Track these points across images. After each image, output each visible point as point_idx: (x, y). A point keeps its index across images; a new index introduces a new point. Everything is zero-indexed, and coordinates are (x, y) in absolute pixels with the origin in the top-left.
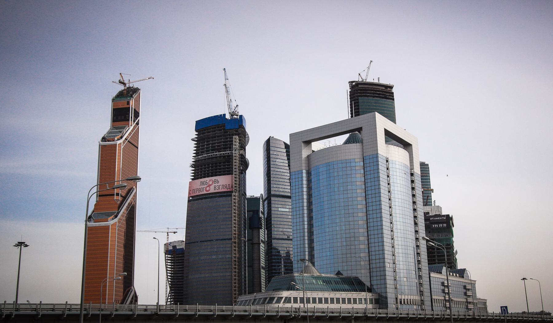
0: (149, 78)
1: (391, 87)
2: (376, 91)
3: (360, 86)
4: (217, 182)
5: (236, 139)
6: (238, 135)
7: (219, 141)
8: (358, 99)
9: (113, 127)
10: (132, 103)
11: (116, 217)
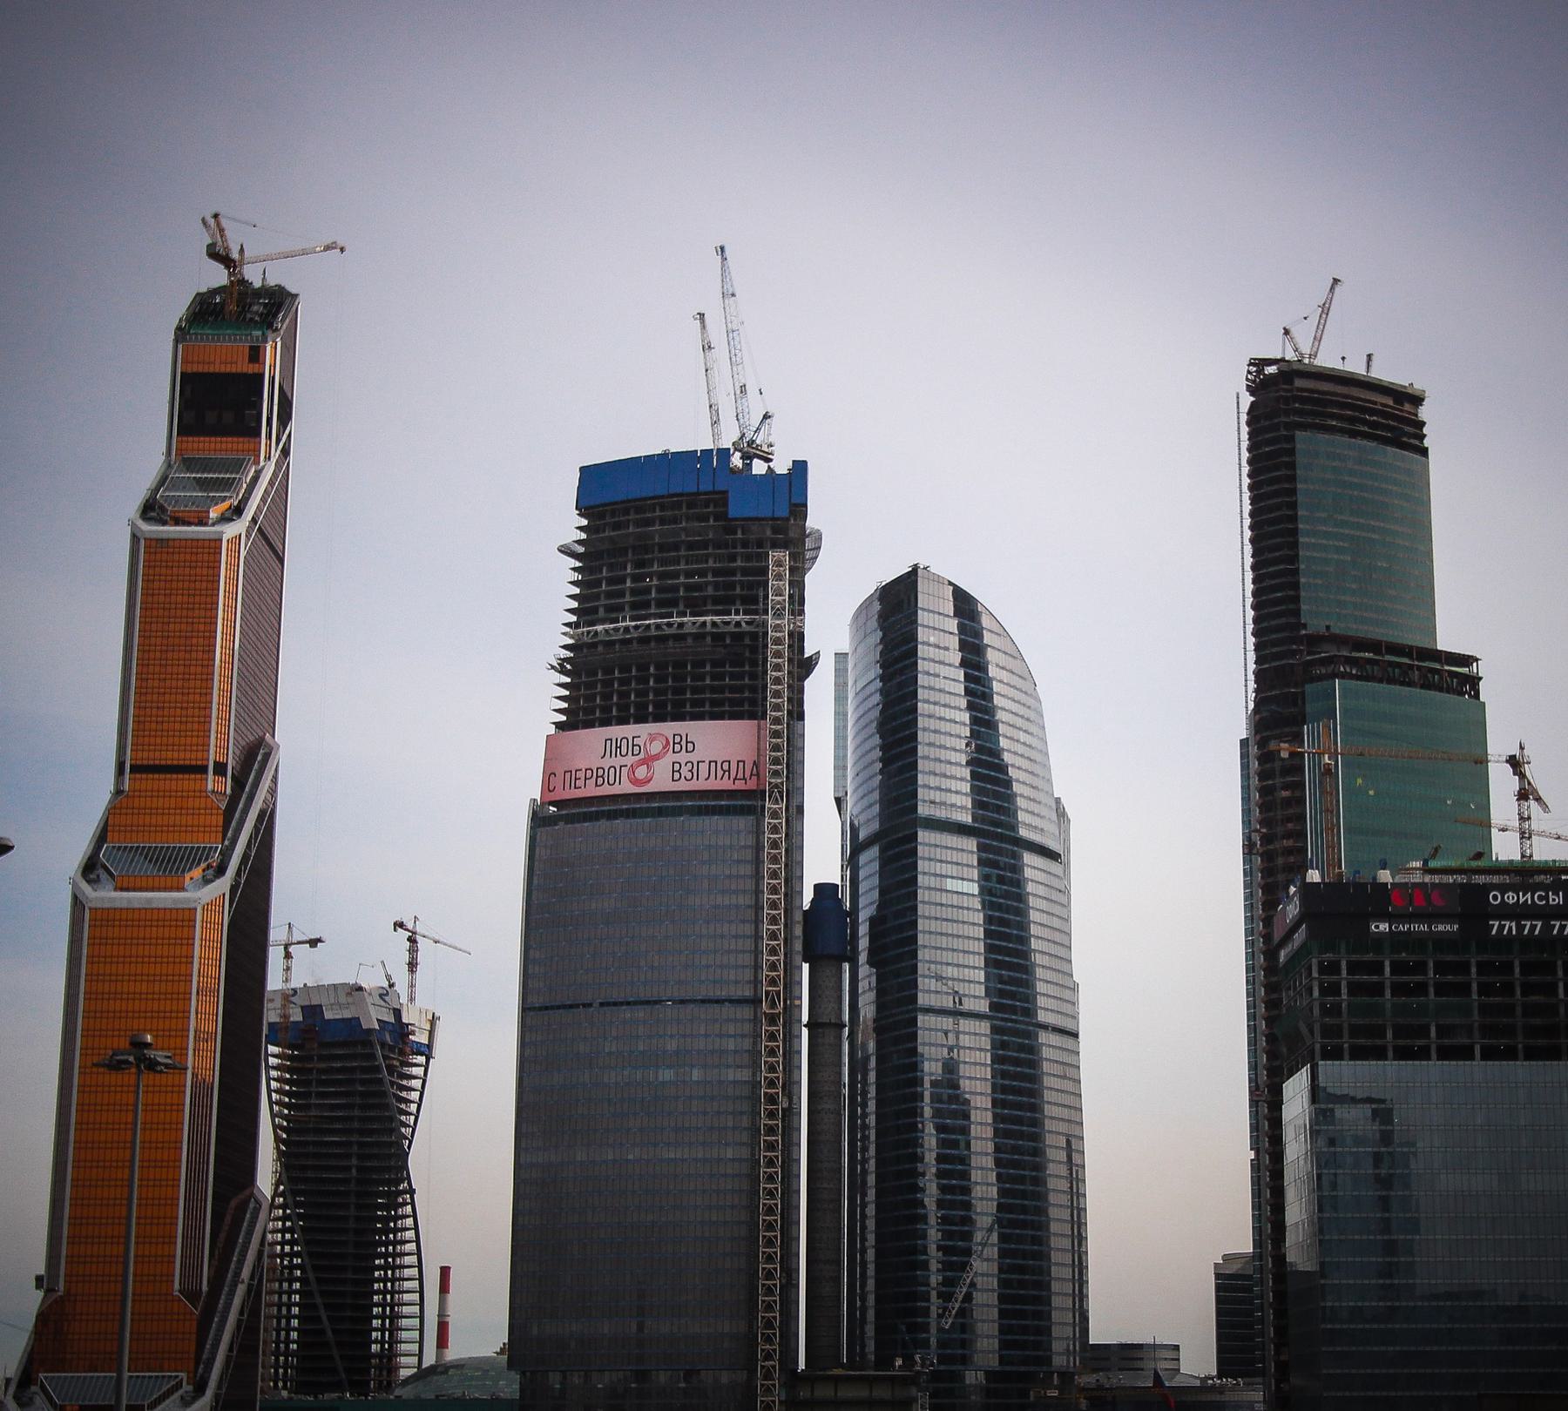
0: (327, 248)
1: (1417, 400)
2: (1364, 410)
3: (1299, 383)
4: (690, 746)
5: (778, 558)
6: (784, 545)
7: (683, 572)
8: (1291, 439)
9: (181, 460)
10: (272, 354)
11: (221, 871)
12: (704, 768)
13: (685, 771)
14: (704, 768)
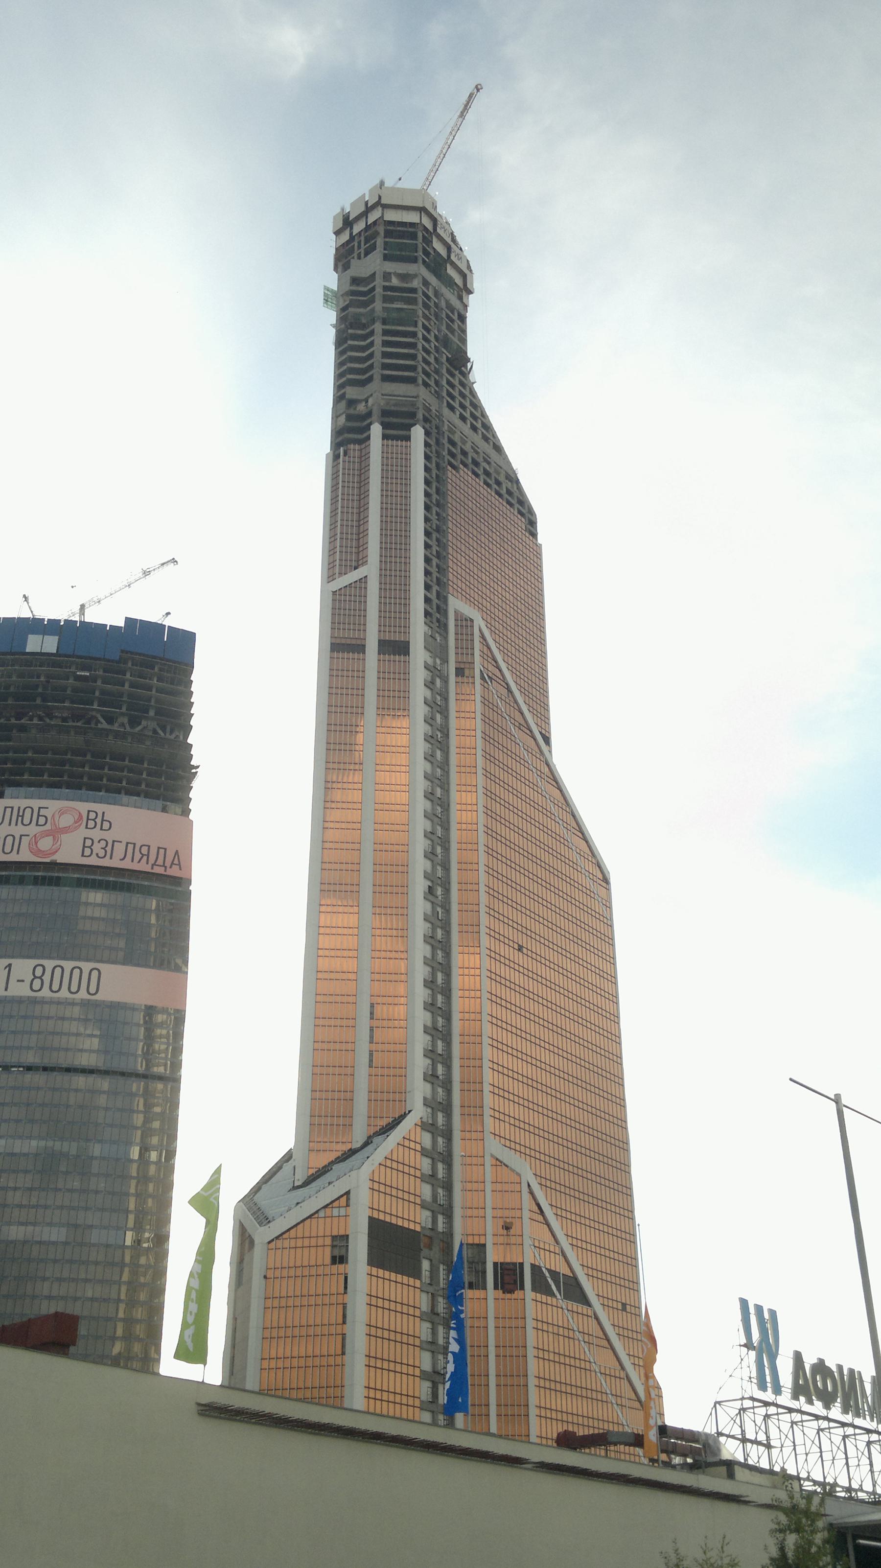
12: (119, 849)
13: (97, 848)
14: (119, 849)
